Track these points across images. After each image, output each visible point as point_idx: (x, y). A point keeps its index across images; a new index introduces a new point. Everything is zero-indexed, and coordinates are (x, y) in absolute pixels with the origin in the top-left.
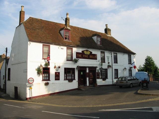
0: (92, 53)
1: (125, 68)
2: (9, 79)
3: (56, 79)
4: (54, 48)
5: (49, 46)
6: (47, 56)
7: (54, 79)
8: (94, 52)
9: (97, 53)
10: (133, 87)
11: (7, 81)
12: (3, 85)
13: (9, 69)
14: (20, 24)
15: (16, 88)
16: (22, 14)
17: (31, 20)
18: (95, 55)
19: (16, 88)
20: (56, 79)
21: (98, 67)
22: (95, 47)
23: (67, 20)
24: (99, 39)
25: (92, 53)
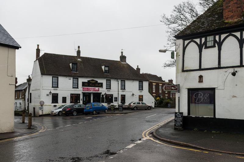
0: (98, 82)
1: (133, 95)
2: (31, 102)
3: (66, 98)
4: (128, 83)
5: (58, 78)
6: (55, 85)
7: (62, 102)
8: (99, 81)
9: (104, 82)
10: (137, 109)
11: (29, 103)
12: (32, 102)
13: (31, 94)
14: (36, 60)
15: (34, 108)
16: (38, 51)
17: (46, 55)
18: (102, 84)
19: (34, 108)
20: (66, 98)
21: (21, 48)
22: (102, 75)
23: (79, 52)
24: (185, 41)
25: (98, 82)
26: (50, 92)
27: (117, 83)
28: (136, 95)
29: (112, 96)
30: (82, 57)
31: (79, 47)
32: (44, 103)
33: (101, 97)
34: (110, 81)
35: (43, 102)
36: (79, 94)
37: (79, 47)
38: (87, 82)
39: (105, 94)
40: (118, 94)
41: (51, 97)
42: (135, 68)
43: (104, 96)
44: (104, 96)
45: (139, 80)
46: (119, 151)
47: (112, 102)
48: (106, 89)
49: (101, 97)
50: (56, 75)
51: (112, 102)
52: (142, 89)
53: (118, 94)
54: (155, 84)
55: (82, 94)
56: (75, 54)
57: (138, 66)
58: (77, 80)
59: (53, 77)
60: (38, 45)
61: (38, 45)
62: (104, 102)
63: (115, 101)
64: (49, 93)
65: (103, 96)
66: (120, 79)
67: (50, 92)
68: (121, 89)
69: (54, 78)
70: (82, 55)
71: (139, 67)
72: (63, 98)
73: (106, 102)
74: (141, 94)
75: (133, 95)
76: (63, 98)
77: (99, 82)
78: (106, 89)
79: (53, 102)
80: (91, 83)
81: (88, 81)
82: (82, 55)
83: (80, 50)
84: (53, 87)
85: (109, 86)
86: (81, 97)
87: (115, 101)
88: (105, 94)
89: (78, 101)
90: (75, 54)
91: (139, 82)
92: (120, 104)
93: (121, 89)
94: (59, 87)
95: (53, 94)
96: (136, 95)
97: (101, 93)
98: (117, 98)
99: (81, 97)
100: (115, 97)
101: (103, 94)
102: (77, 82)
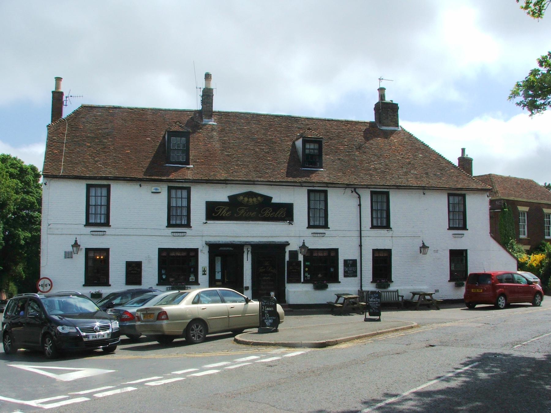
0: (273, 201)
1: (424, 248)
3: (138, 265)
20: (138, 265)
25: (273, 201)
26: (76, 245)
27: (355, 202)
28: (436, 251)
29: (333, 254)
30: (220, 113)
31: (208, 77)
32: (51, 285)
33: (287, 258)
34: (322, 198)
35: (47, 282)
36: (196, 251)
37: (208, 77)
38: (226, 200)
39: (304, 246)
40: (361, 246)
41: (80, 259)
42: (453, 158)
43: (301, 258)
44: (301, 258)
45: (450, 189)
46: (497, 324)
47: (335, 280)
48: (310, 227)
49: (287, 258)
50: (101, 178)
51: (335, 280)
52: (322, 223)
53: (361, 246)
54: (526, 209)
55: (206, 249)
56: (195, 104)
57: (463, 150)
58: (185, 193)
59: (89, 187)
60: (58, 80)
61: (58, 80)
62: (298, 281)
63: (346, 275)
64: (70, 249)
65: (293, 254)
66: (367, 187)
67: (76, 245)
68: (373, 227)
69: (93, 191)
70: (218, 105)
71: (469, 154)
72: (129, 265)
73: (306, 281)
74: (458, 245)
75: (424, 248)
76: (129, 265)
77: (276, 200)
78: (310, 227)
79: (88, 282)
80: (241, 204)
81: (229, 197)
82: (218, 105)
83: (213, 85)
84: (88, 224)
85: (322, 215)
86: (203, 261)
87: (346, 275)
88: (304, 246)
89: (192, 278)
90: (195, 104)
91: (449, 195)
92: (369, 287)
93: (373, 227)
94: (330, 225)
95: (88, 250)
96: (436, 251)
97: (287, 244)
98: (355, 261)
99: (203, 261)
100: (346, 262)
101: (294, 246)
102: (104, 202)
